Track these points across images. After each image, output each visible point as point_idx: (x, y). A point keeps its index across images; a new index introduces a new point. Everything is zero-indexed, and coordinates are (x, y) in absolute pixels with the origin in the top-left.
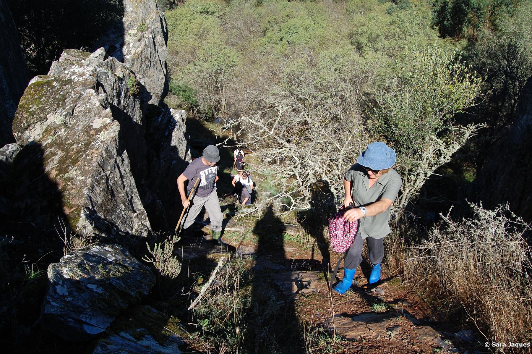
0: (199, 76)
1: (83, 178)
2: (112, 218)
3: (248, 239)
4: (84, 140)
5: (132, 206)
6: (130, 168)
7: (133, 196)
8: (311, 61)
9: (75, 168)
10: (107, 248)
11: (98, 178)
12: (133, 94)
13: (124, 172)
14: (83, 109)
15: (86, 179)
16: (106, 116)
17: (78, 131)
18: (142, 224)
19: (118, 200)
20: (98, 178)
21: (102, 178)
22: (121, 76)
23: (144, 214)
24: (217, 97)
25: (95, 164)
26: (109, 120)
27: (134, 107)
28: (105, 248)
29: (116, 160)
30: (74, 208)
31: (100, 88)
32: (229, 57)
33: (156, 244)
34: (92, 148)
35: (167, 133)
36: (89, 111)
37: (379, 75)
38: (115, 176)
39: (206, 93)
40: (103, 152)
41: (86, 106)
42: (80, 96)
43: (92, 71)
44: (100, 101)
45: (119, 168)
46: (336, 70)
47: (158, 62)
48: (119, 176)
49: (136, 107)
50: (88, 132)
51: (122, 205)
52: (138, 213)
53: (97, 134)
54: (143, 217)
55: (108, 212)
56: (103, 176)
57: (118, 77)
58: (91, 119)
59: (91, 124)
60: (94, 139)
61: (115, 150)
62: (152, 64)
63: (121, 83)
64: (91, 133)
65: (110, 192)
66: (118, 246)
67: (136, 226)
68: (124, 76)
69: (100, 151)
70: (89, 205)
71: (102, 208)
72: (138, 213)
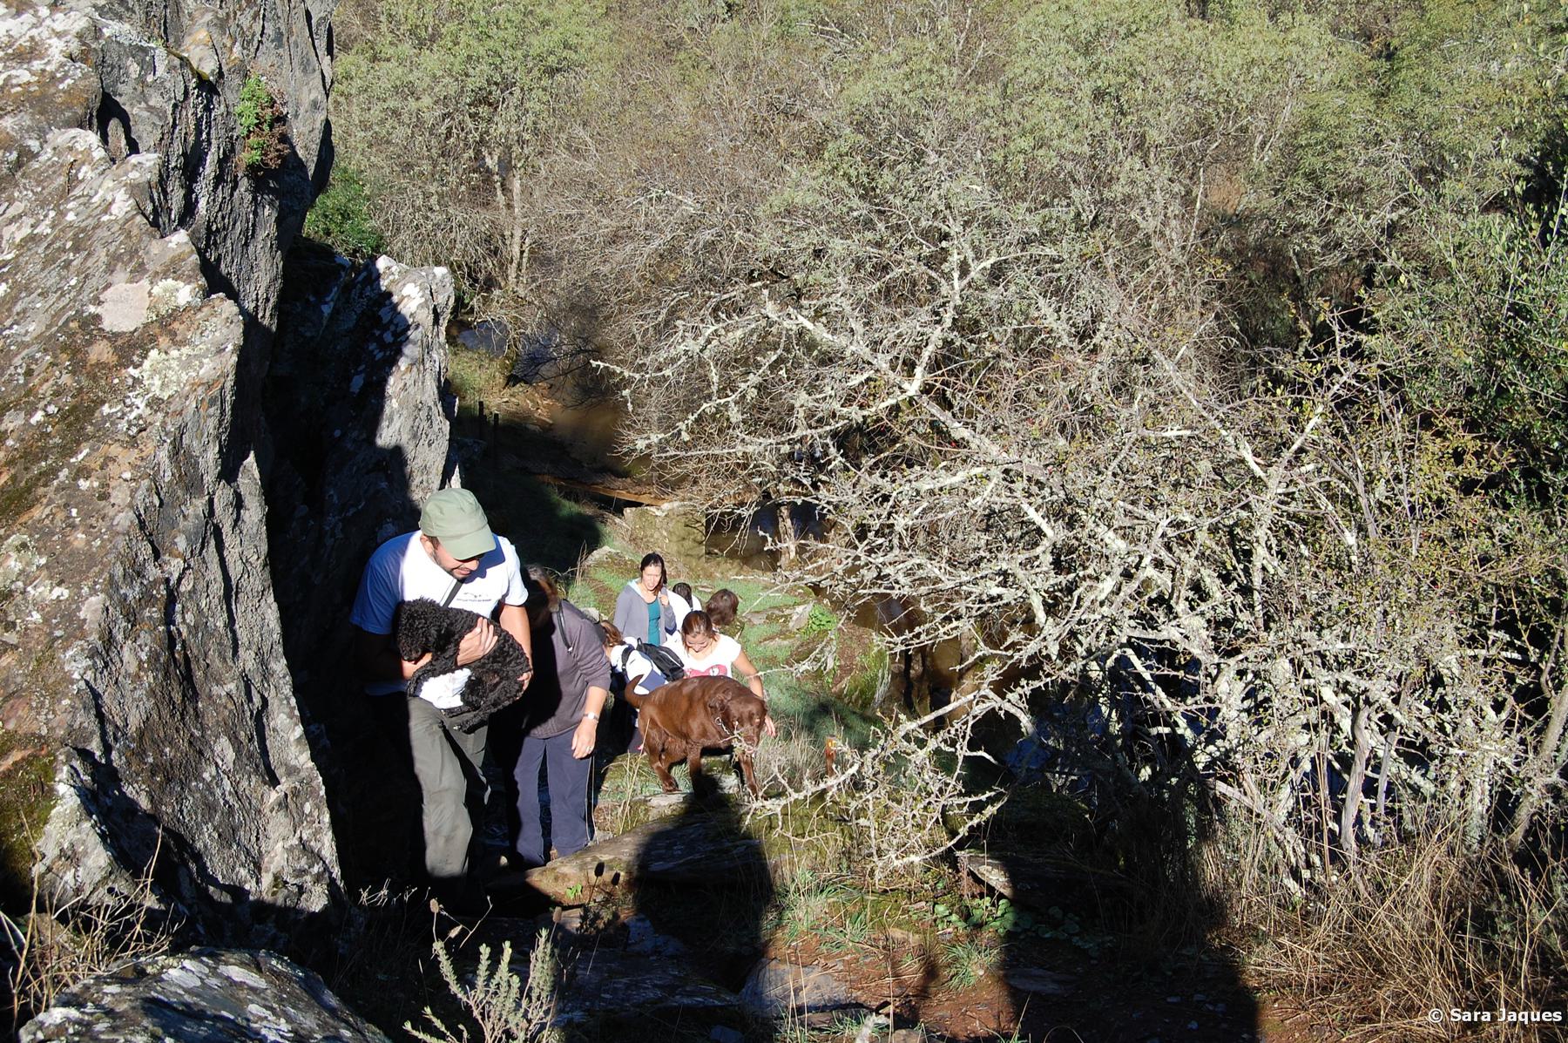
0: (396, 113)
1: (62, 592)
2: (182, 810)
3: (804, 926)
4: (57, 394)
5: (264, 752)
6: (264, 548)
7: (271, 695)
8: (968, 50)
9: (14, 540)
10: (236, 973)
11: (133, 593)
12: (252, 169)
13: (240, 568)
14: (44, 229)
15: (77, 600)
16: (172, 269)
17: (27, 345)
18: (304, 846)
19: (211, 718)
20: (133, 593)
21: (147, 598)
22: (208, 68)
23: (313, 793)
24: (481, 219)
25: (125, 519)
26: (185, 293)
27: (249, 237)
28: (222, 969)
29: (211, 501)
30: (16, 756)
31: (114, 126)
32: (545, 23)
33: (485, 950)
34: (103, 434)
35: (358, 382)
36: (75, 238)
37: (1314, 126)
38: (201, 585)
39: (427, 196)
40: (163, 455)
41: (62, 214)
42: (19, 164)
43: (80, 36)
44: (133, 189)
45: (220, 547)
46: (1099, 95)
47: (300, 24)
48: (217, 588)
49: (261, 234)
50: (76, 353)
51: (224, 741)
52: (285, 785)
53: (125, 360)
54: (308, 808)
55: (169, 780)
56: (155, 583)
57: (199, 76)
58: (93, 282)
59: (92, 309)
60: (114, 390)
61: (213, 452)
62: (269, 30)
63: (207, 109)
64: (93, 357)
65: (179, 672)
66: (279, 959)
67: (277, 856)
68: (221, 74)
69: (149, 449)
70: (88, 740)
71: (140, 754)
72: (285, 785)
